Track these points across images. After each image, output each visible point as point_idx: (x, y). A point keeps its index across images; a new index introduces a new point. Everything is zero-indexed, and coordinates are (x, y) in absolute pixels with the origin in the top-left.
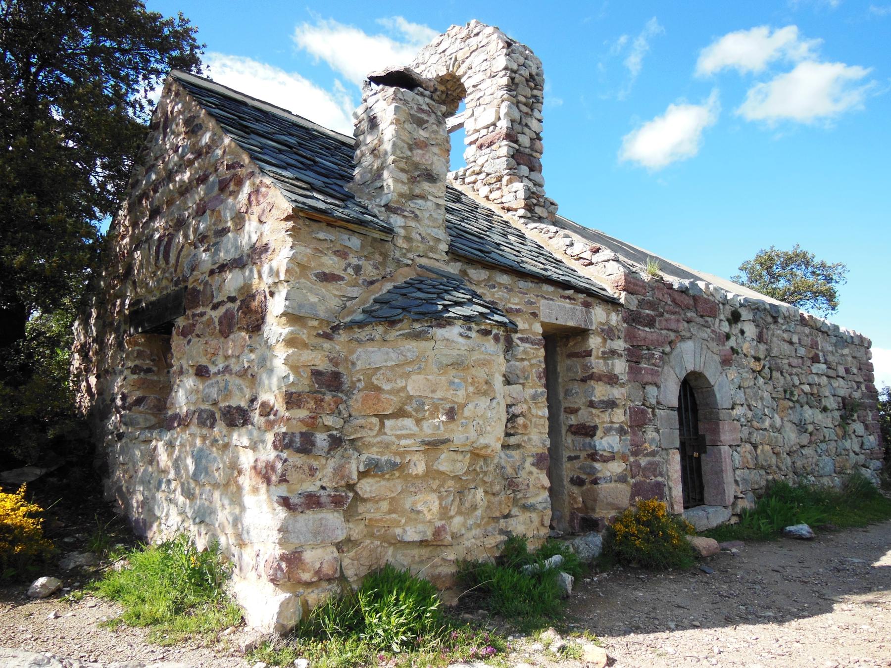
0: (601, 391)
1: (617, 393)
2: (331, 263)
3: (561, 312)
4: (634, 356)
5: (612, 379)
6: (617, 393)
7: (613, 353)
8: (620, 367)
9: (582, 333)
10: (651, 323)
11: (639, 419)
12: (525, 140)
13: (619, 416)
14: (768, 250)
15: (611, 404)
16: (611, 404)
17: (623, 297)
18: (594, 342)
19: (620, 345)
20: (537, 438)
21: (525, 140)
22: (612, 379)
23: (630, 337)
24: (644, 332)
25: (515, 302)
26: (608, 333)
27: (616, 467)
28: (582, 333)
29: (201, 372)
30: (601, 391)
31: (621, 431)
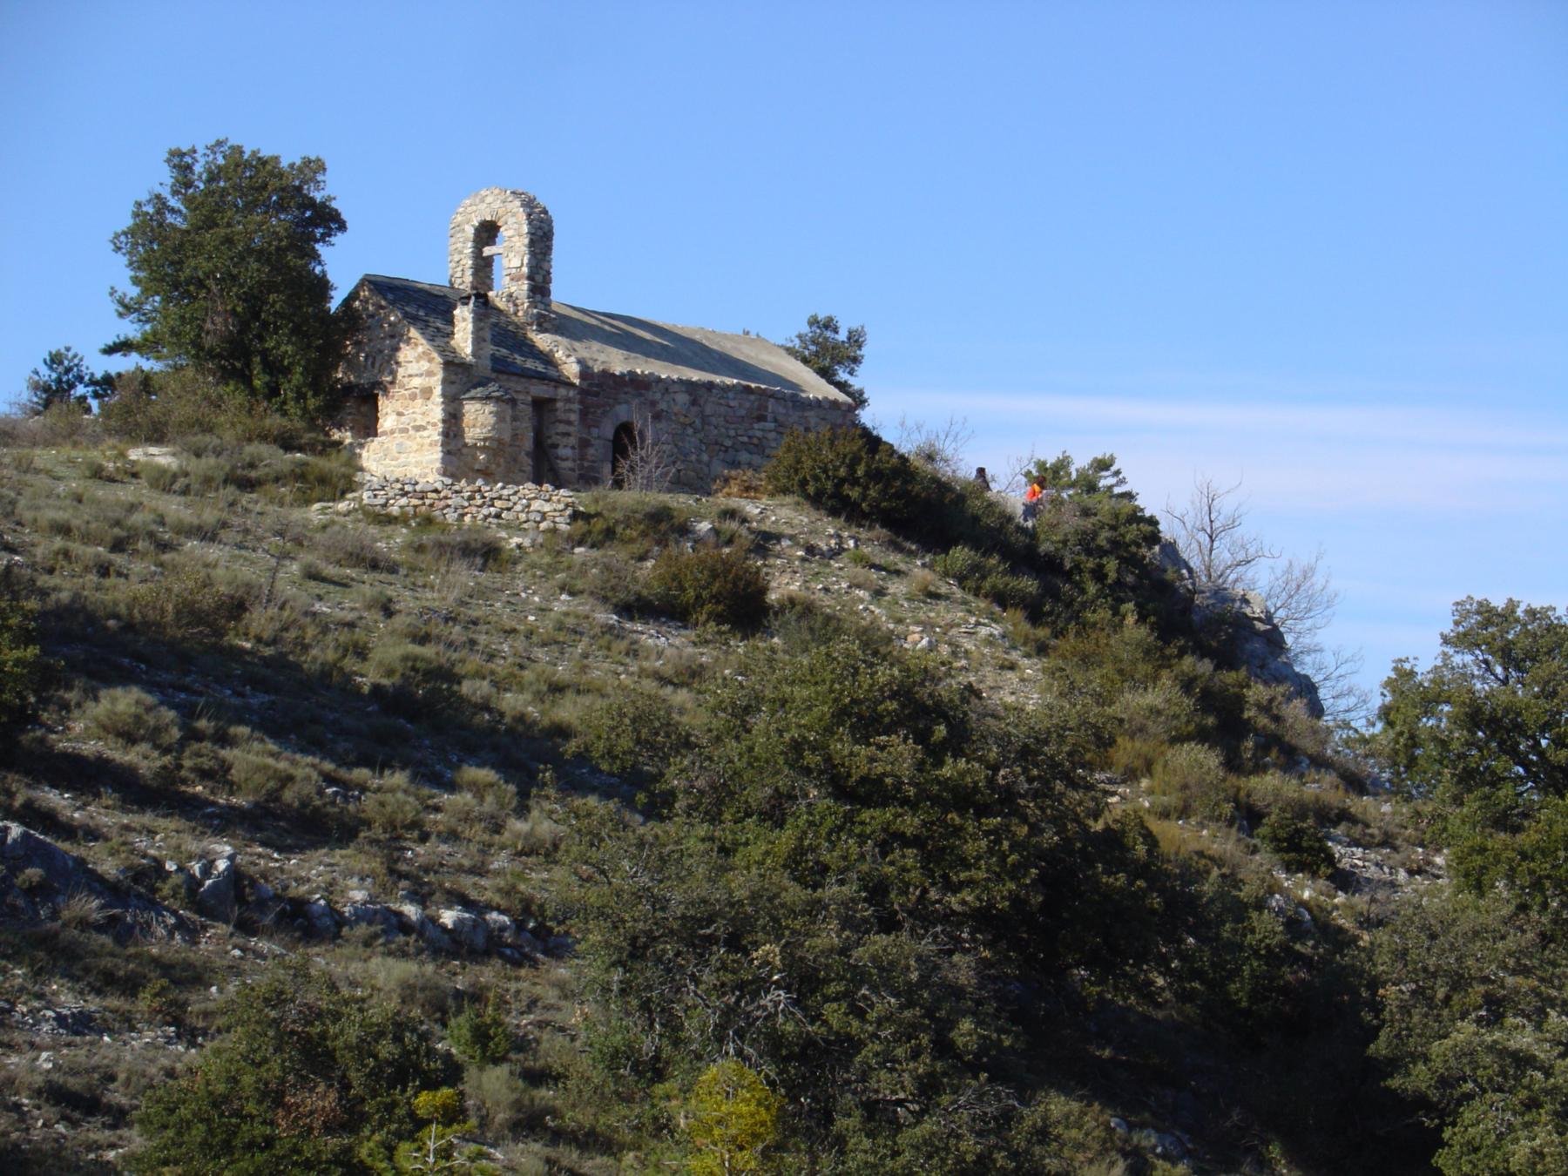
0: (562, 428)
1: (571, 429)
2: (453, 378)
3: (540, 390)
4: (584, 414)
5: (569, 423)
6: (571, 429)
7: (570, 410)
8: (574, 417)
9: (552, 401)
10: (597, 394)
11: (584, 444)
12: (539, 278)
13: (572, 441)
14: (805, 329)
15: (568, 434)
16: (568, 434)
17: (577, 381)
18: (559, 405)
19: (576, 406)
20: (528, 444)
21: (539, 278)
22: (569, 423)
23: (581, 402)
24: (590, 399)
25: (519, 388)
26: (568, 400)
27: (569, 464)
28: (552, 401)
29: (400, 414)
30: (562, 428)
31: (573, 448)
